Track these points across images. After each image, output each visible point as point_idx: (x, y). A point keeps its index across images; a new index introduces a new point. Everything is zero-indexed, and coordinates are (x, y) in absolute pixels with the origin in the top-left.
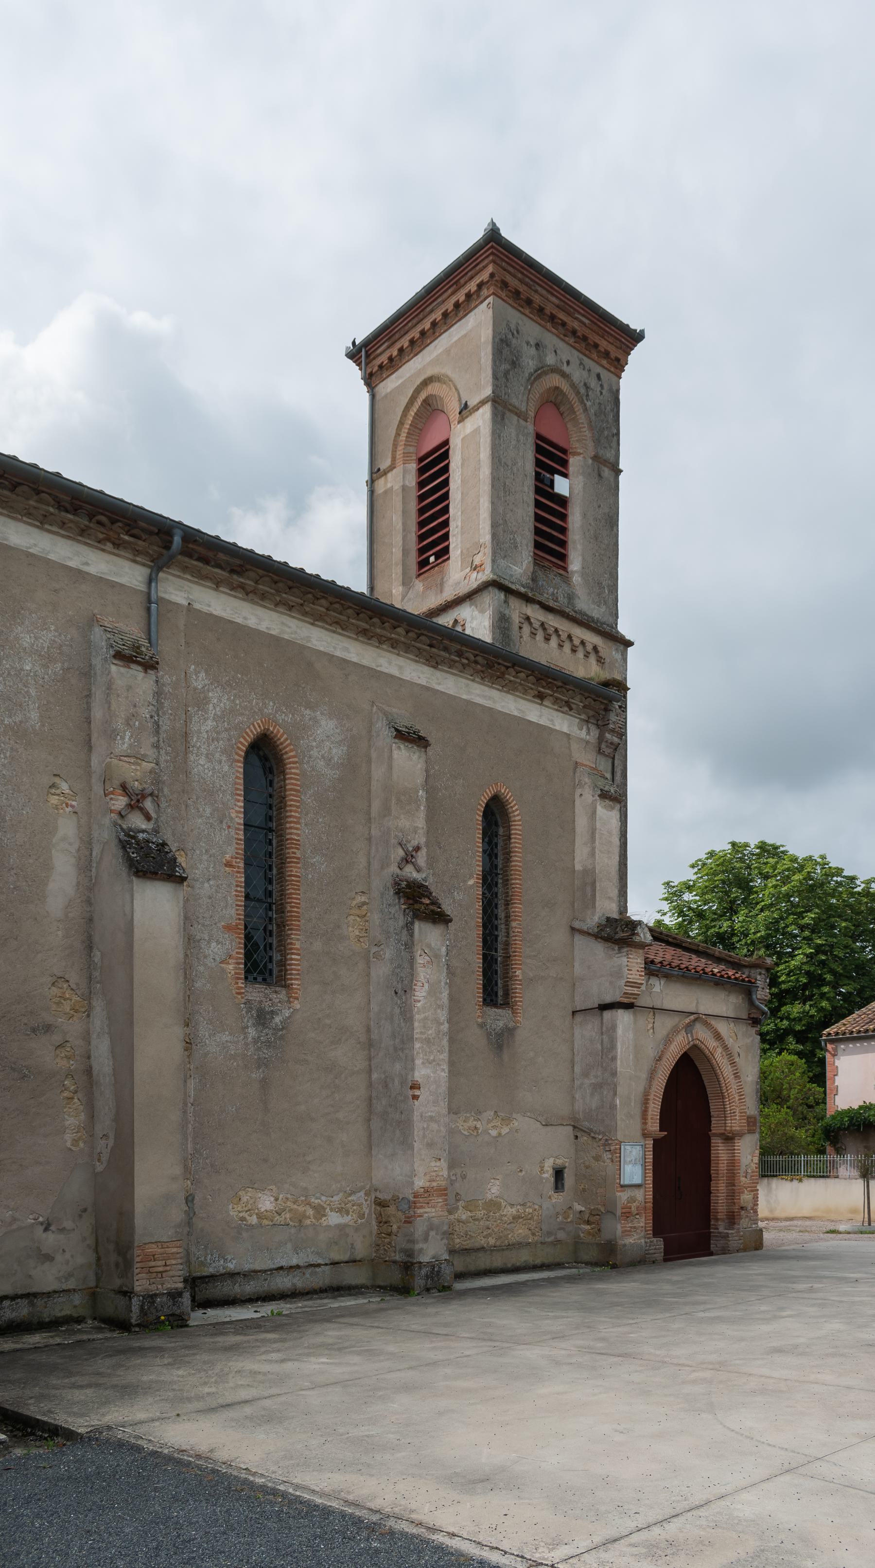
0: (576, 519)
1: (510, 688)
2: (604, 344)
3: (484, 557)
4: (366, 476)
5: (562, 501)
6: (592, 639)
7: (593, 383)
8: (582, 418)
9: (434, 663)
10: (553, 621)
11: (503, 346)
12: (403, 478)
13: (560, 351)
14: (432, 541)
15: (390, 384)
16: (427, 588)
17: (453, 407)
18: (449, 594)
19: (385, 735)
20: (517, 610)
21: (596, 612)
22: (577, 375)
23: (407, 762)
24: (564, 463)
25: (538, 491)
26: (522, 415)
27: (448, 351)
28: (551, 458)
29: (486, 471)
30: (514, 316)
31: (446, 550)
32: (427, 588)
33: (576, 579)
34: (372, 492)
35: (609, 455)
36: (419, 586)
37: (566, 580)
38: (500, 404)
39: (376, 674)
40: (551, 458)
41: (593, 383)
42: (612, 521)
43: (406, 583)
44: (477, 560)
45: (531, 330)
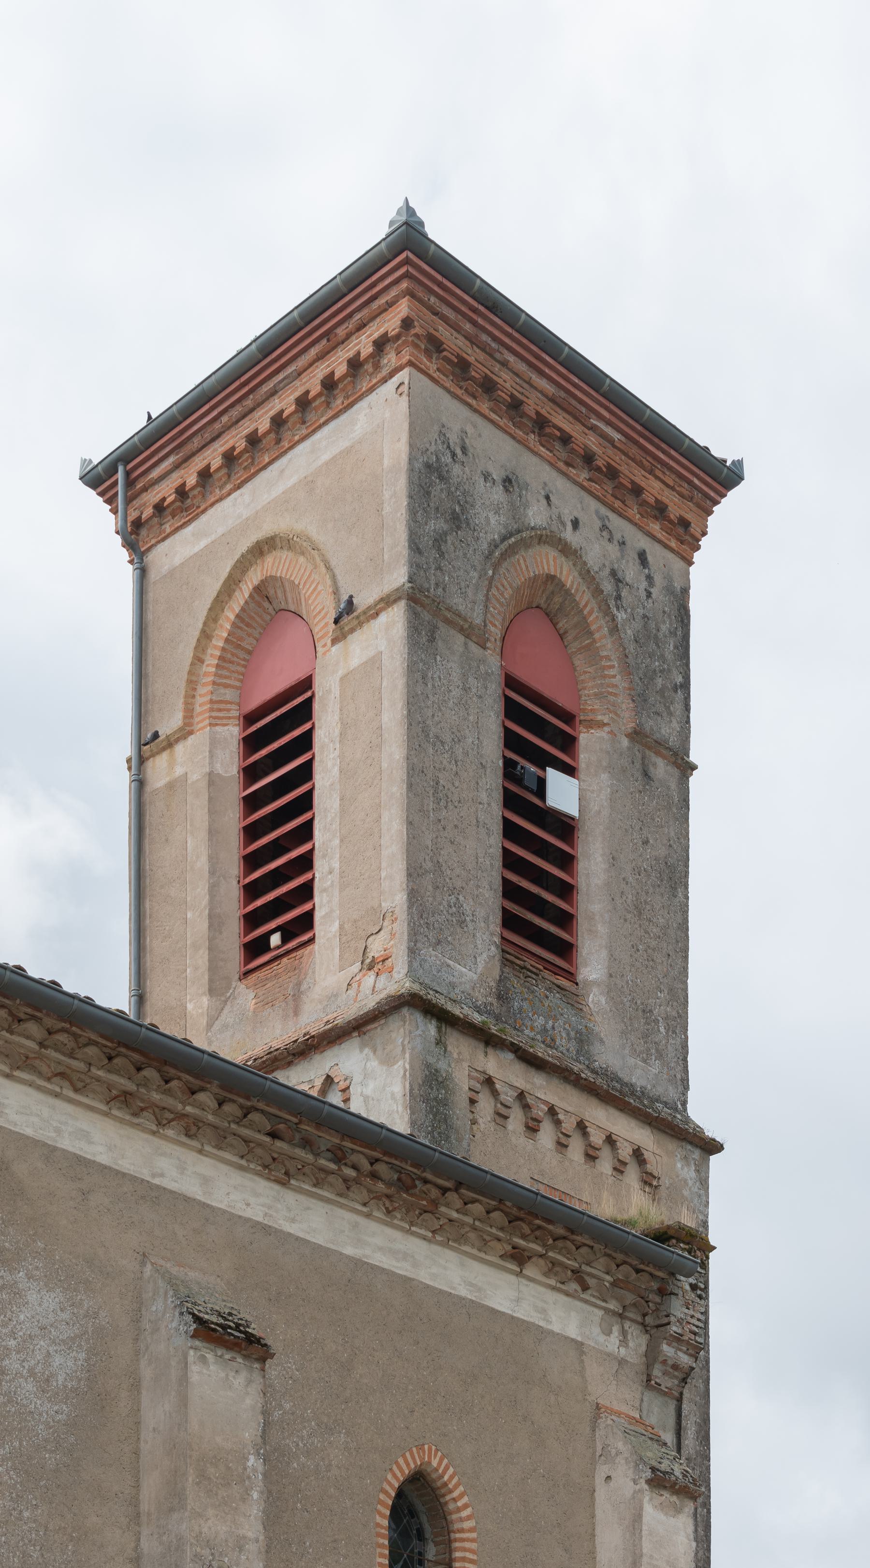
0: (594, 868)
1: (450, 1235)
2: (653, 488)
3: (391, 941)
4: (122, 744)
5: (564, 826)
6: (632, 1133)
7: (631, 572)
8: (606, 645)
9: (280, 1172)
10: (545, 1090)
11: (433, 480)
12: (208, 758)
13: (557, 498)
14: (276, 903)
15: (178, 549)
16: (265, 1003)
17: (321, 608)
18: (312, 1019)
19: (170, 1330)
20: (465, 1061)
21: (640, 1074)
22: (596, 552)
23: (221, 1389)
24: (568, 743)
25: (510, 801)
26: (474, 634)
27: (309, 483)
28: (537, 732)
29: (394, 752)
30: (456, 415)
31: (306, 922)
32: (265, 1003)
33: (596, 999)
34: (140, 784)
35: (667, 730)
36: (246, 996)
37: (574, 999)
38: (425, 606)
39: (154, 1195)
40: (537, 732)
41: (631, 572)
42: (674, 875)
43: (217, 988)
44: (376, 948)
45: (494, 447)
